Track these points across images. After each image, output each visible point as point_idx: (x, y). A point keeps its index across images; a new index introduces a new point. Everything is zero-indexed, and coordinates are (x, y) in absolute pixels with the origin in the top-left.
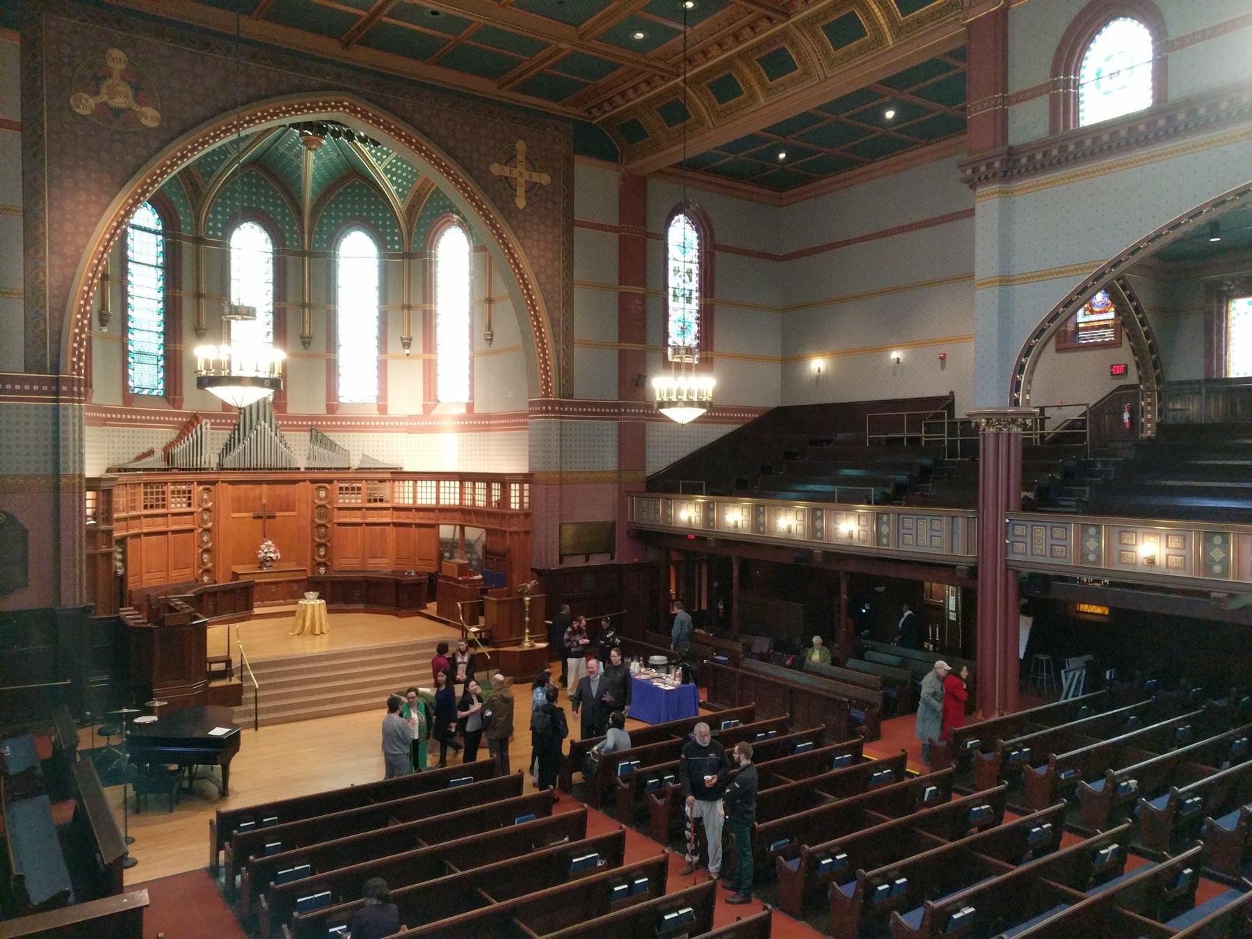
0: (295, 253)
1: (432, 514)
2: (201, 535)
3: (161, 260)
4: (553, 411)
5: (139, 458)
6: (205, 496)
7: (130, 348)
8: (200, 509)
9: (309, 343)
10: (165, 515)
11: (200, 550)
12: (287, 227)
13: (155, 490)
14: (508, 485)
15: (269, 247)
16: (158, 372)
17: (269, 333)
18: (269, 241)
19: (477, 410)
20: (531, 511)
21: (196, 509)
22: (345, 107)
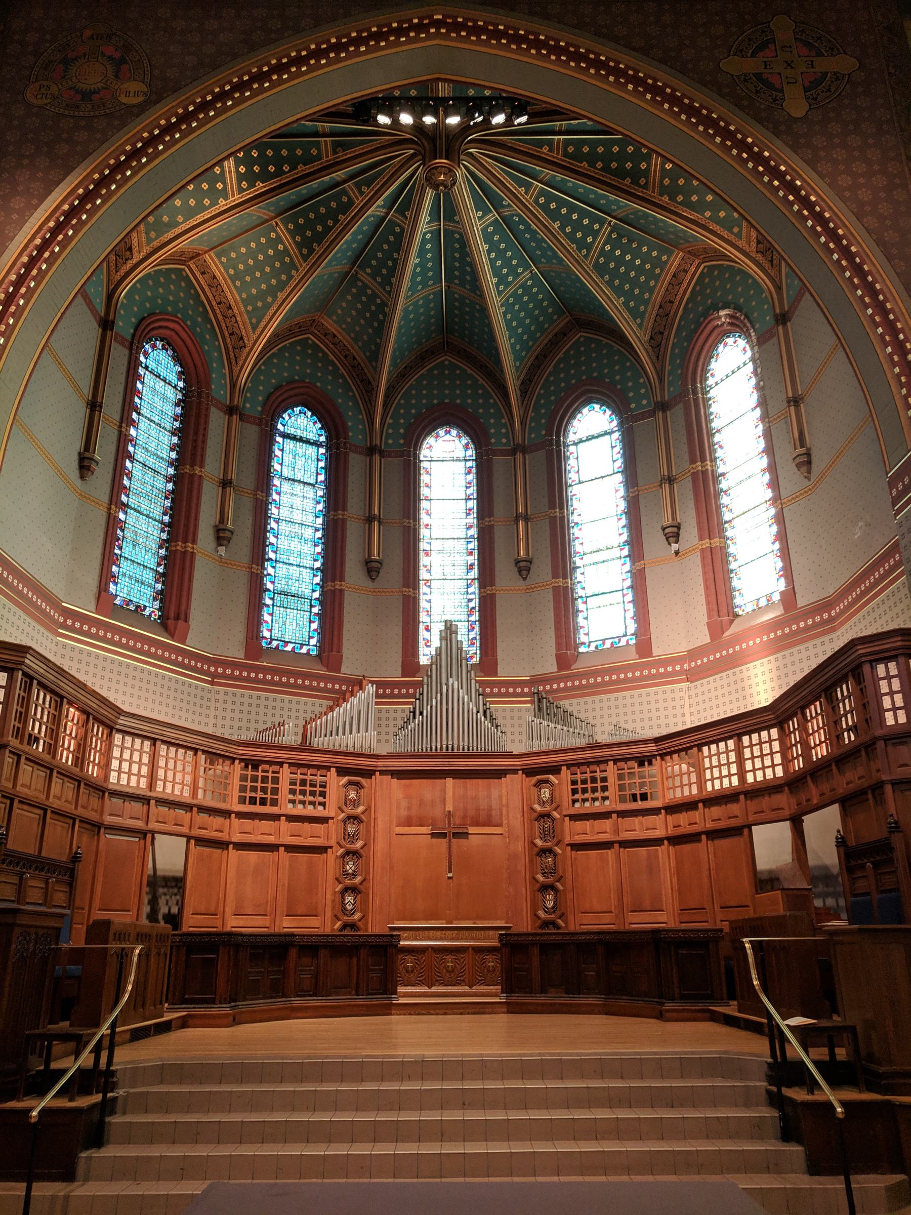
0: (503, 453)
1: (734, 808)
3: (321, 478)
6: (352, 795)
8: (342, 816)
9: (528, 570)
10: (275, 817)
11: (339, 887)
12: (492, 421)
13: (260, 774)
14: (866, 668)
17: (472, 565)
18: (471, 446)
19: (802, 601)
21: (332, 814)
22: (438, 24)
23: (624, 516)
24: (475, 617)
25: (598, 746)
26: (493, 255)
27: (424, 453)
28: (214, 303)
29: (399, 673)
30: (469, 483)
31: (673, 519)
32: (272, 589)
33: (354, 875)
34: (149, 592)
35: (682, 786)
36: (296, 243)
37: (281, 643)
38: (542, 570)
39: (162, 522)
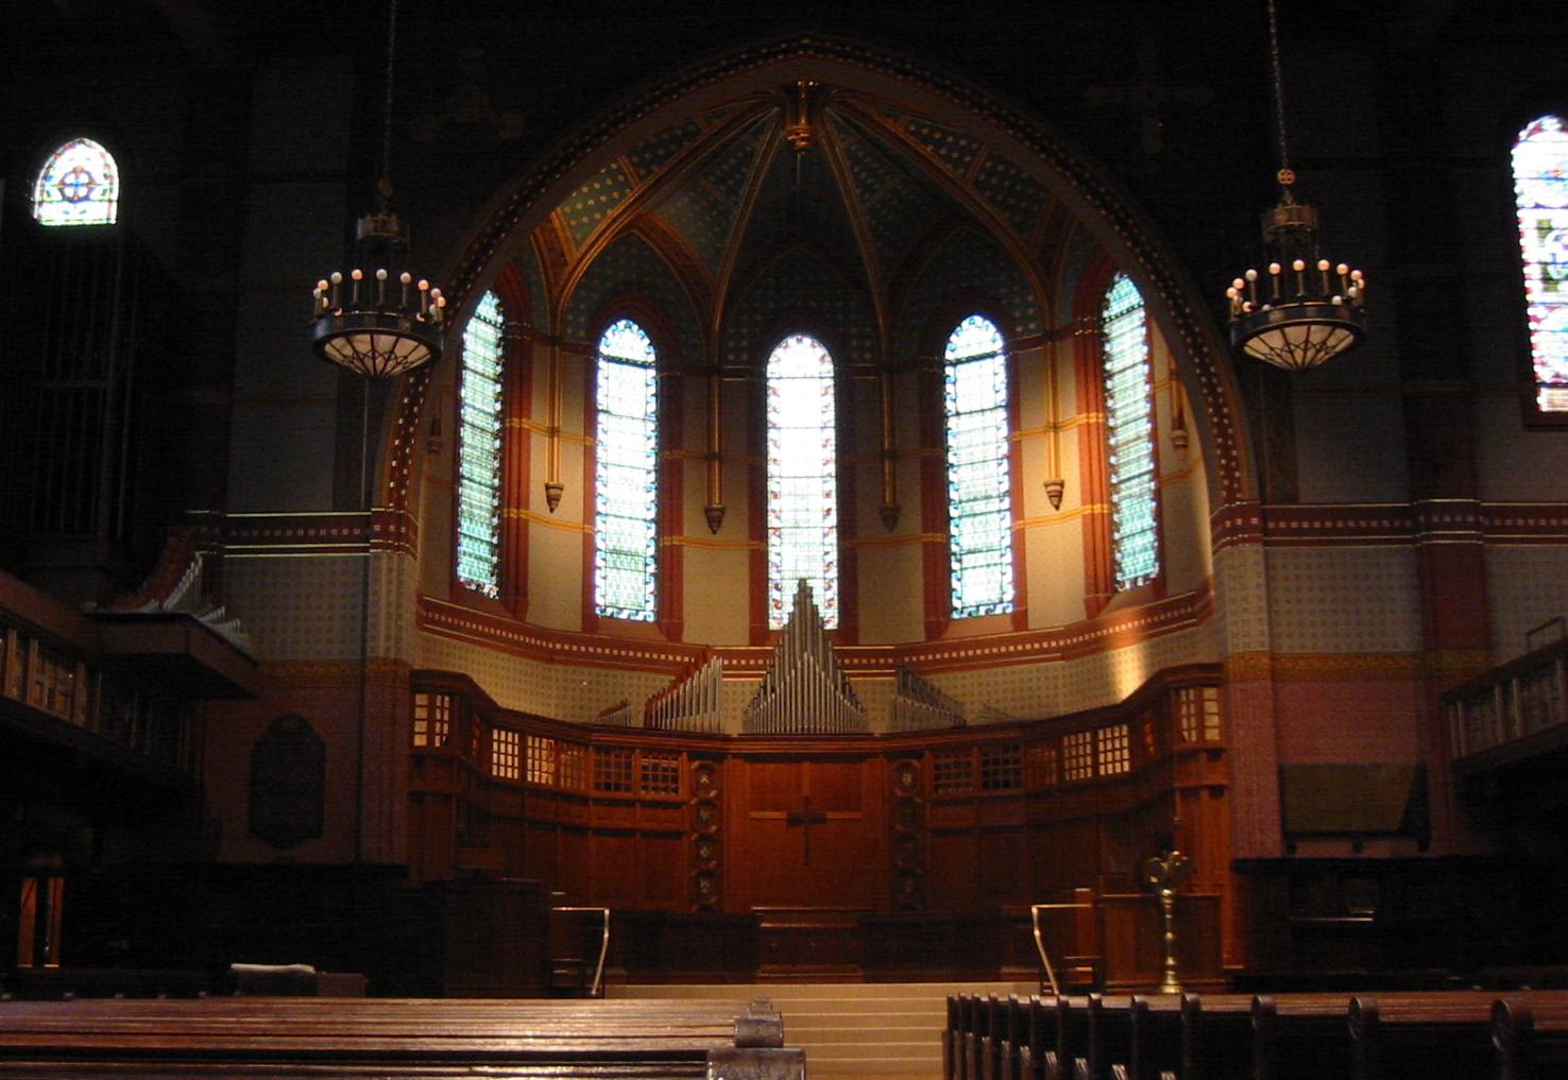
2: (697, 845)
4: (1246, 528)
5: (602, 714)
7: (600, 544)
10: (630, 803)
11: (694, 873)
15: (828, 368)
16: (646, 583)
17: (829, 510)
18: (828, 359)
20: (1224, 746)
21: (685, 798)
22: (806, 47)
23: (1005, 462)
24: (833, 573)
25: (961, 727)
26: (856, 169)
27: (772, 368)
28: (544, 248)
29: (747, 641)
30: (826, 407)
31: (1056, 477)
32: (603, 548)
33: (709, 860)
34: (486, 567)
35: (1078, 768)
36: (633, 164)
37: (615, 610)
38: (912, 521)
39: (492, 487)
